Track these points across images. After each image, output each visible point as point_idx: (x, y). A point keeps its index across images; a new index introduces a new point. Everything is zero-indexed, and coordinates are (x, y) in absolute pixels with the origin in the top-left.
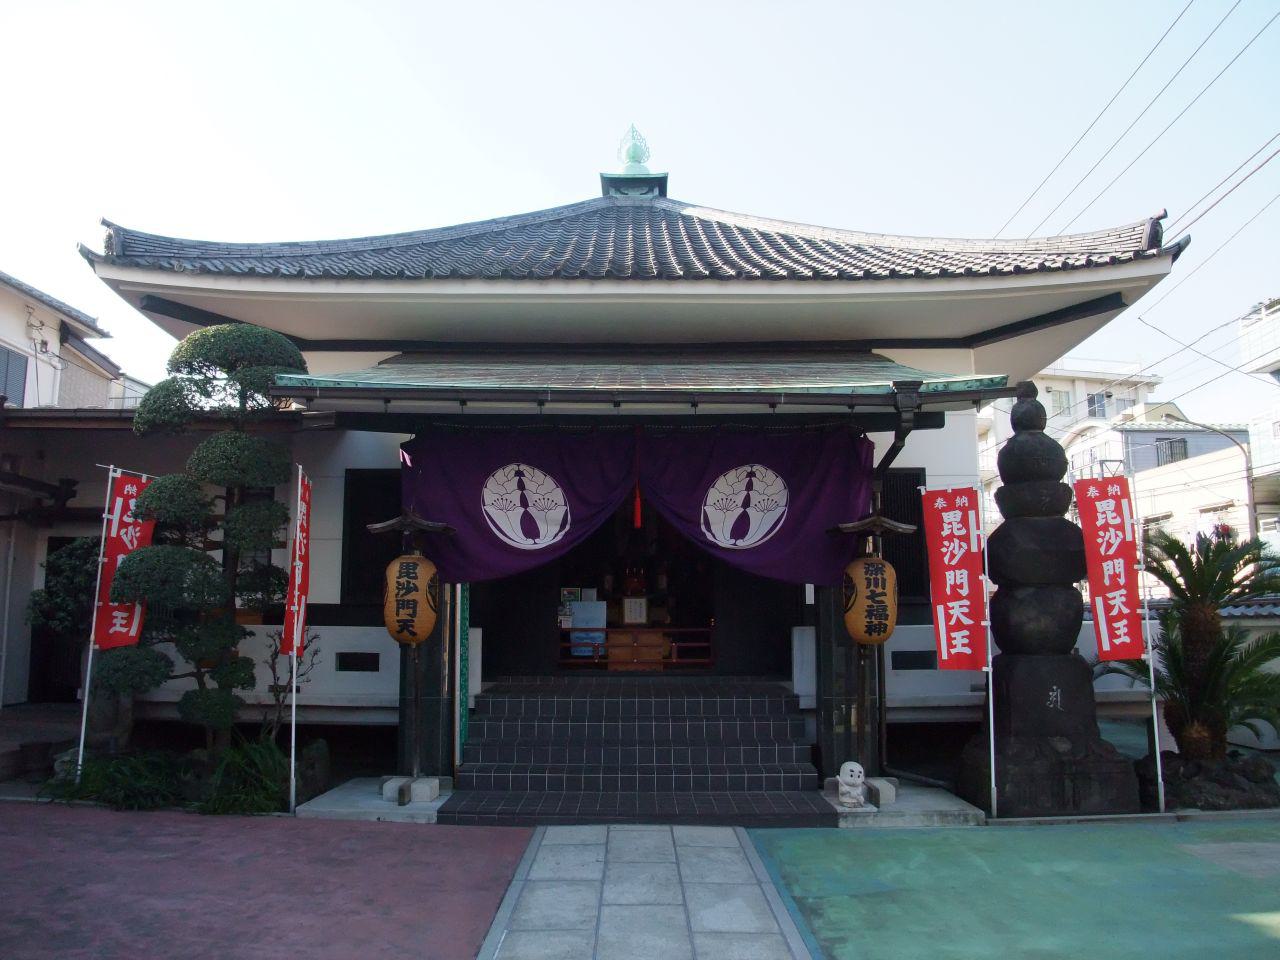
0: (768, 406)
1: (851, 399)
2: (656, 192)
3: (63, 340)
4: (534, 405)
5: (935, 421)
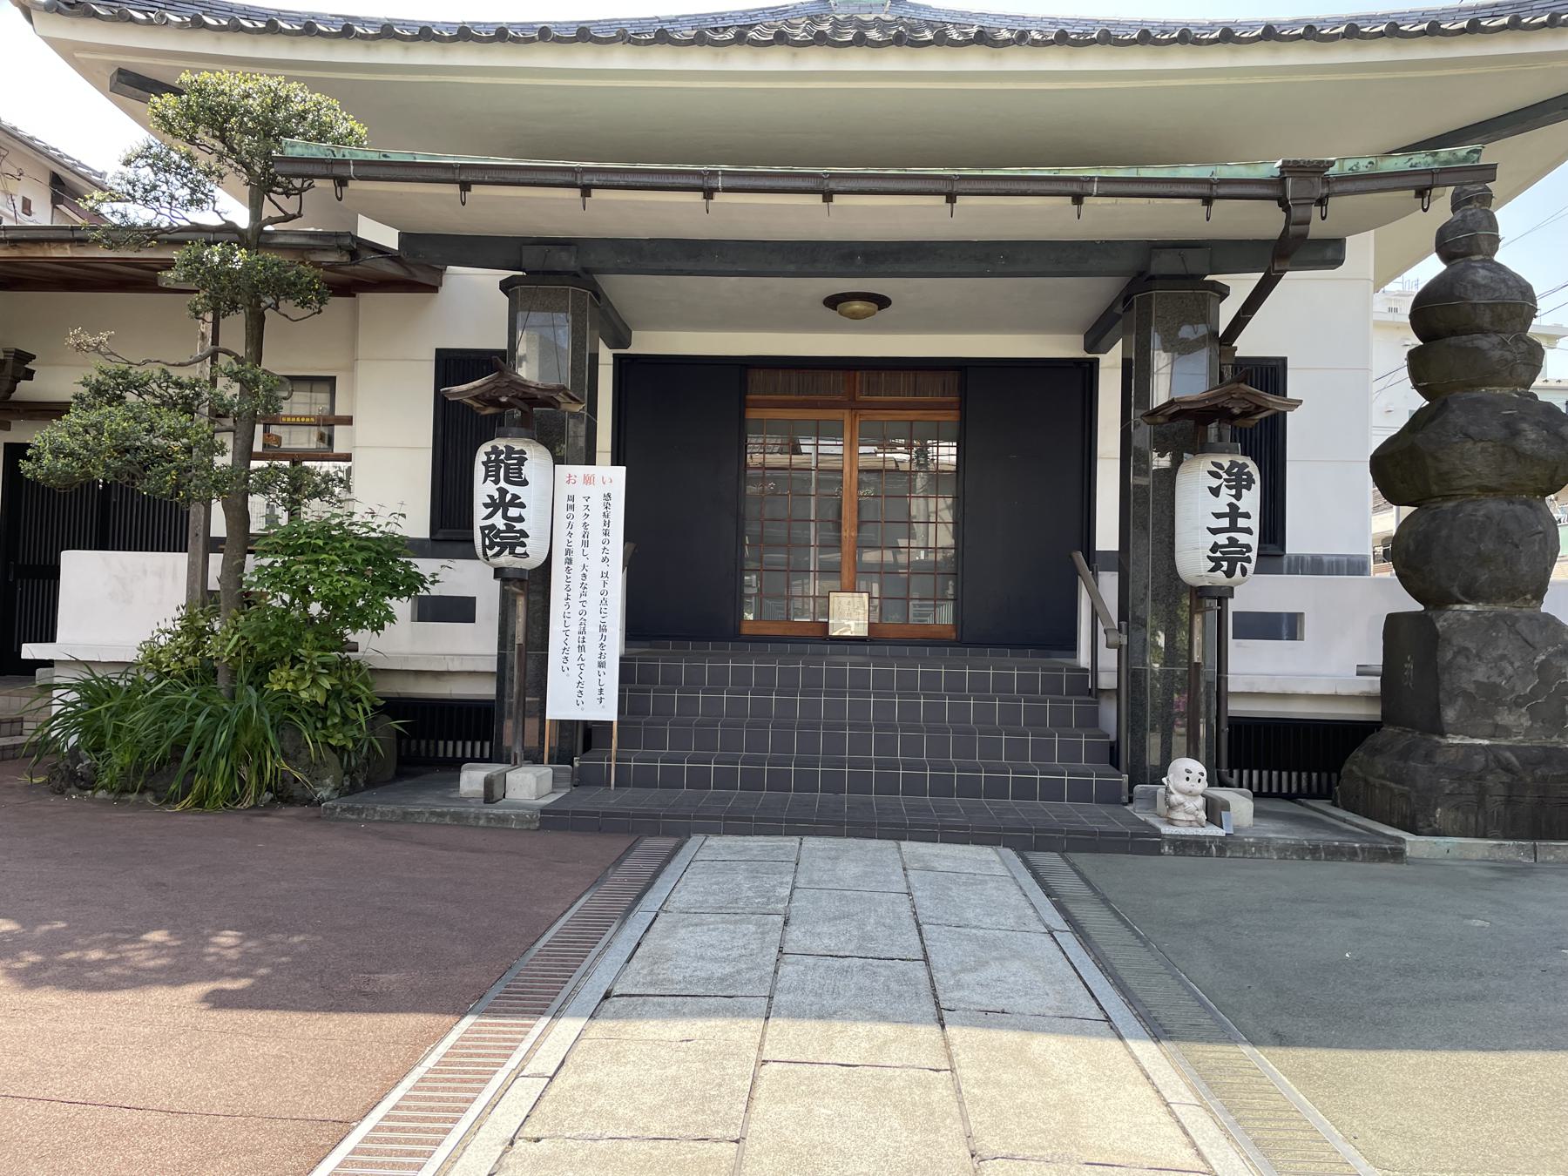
0: (820, 197)
3: (56, 200)
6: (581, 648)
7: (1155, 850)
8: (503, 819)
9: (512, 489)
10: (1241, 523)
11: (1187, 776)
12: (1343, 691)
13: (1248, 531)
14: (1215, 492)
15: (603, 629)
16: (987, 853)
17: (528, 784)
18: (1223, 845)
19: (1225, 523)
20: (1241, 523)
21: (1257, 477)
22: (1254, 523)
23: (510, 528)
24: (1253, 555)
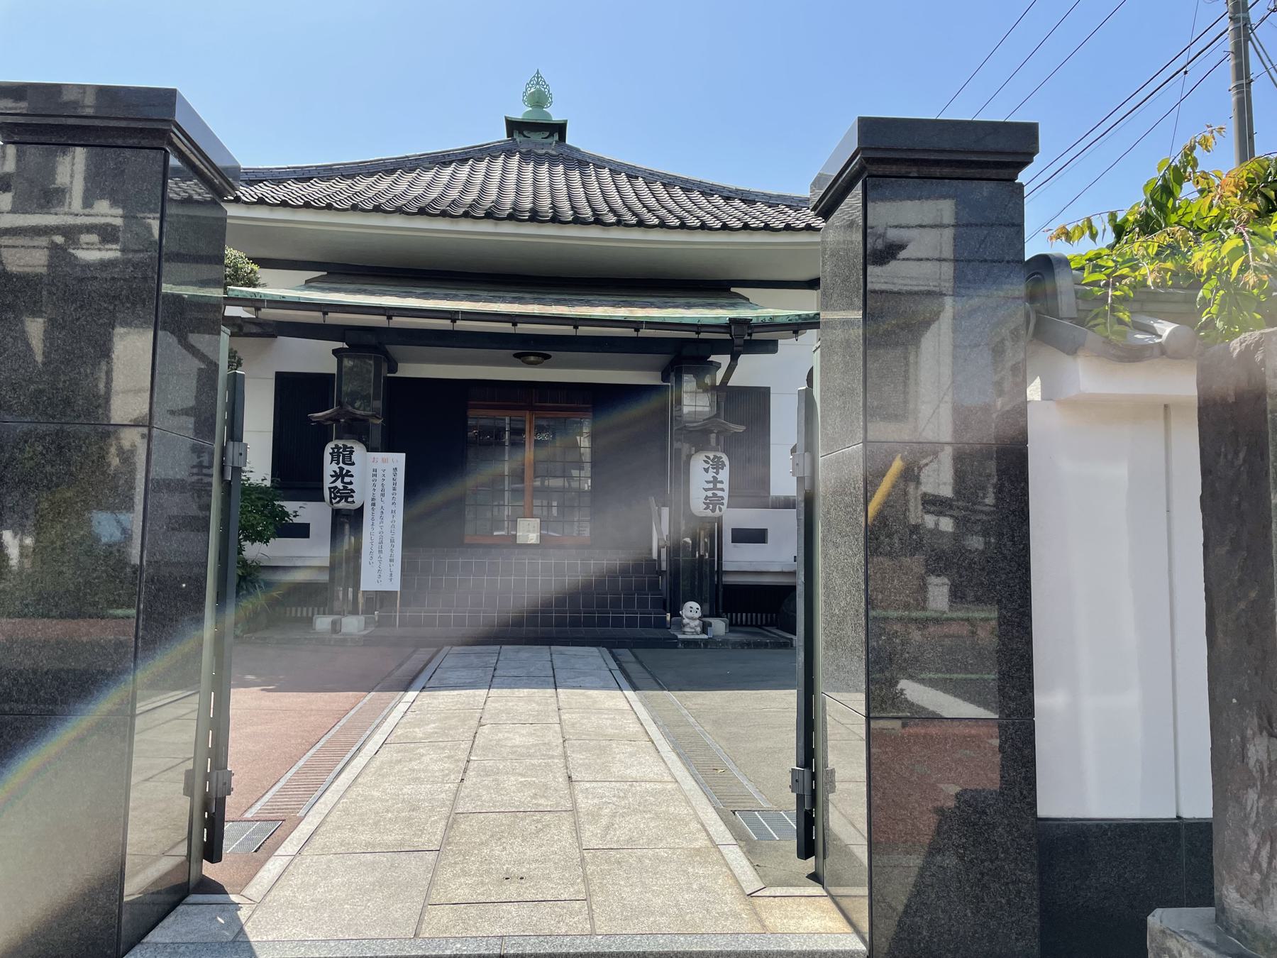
1: (698, 327)
2: (556, 137)
4: (448, 322)
5: (769, 347)
6: (380, 552)
7: (675, 646)
8: (344, 640)
9: (346, 467)
10: (719, 486)
11: (691, 609)
12: (786, 569)
13: (722, 490)
14: (706, 470)
15: (392, 541)
16: (594, 650)
17: (353, 624)
18: (706, 643)
19: (711, 486)
20: (719, 486)
21: (727, 463)
22: (726, 486)
23: (345, 488)
24: (725, 501)
